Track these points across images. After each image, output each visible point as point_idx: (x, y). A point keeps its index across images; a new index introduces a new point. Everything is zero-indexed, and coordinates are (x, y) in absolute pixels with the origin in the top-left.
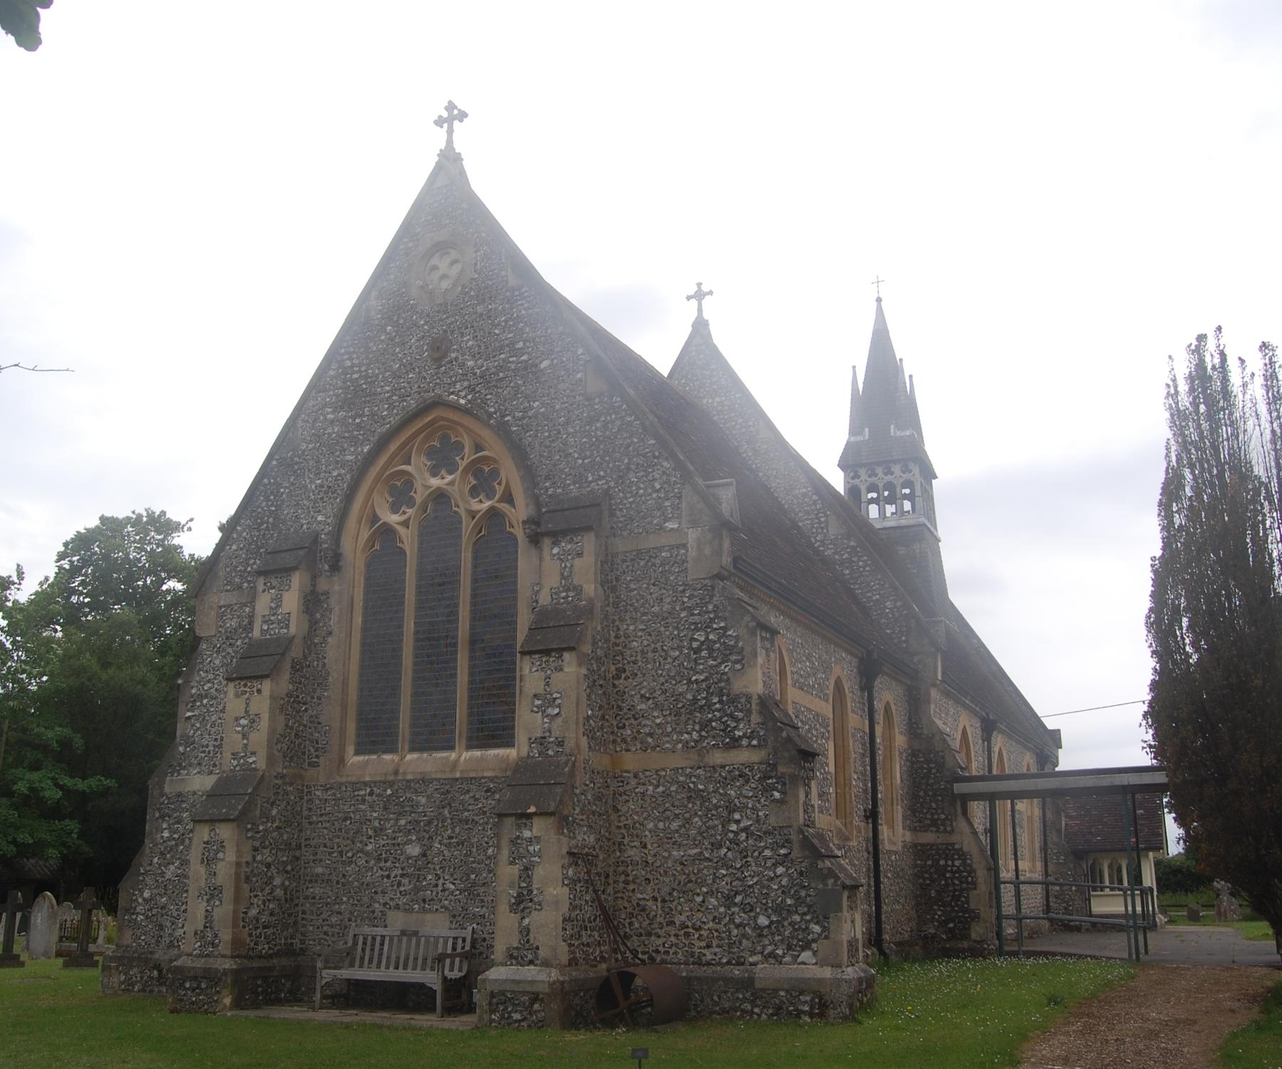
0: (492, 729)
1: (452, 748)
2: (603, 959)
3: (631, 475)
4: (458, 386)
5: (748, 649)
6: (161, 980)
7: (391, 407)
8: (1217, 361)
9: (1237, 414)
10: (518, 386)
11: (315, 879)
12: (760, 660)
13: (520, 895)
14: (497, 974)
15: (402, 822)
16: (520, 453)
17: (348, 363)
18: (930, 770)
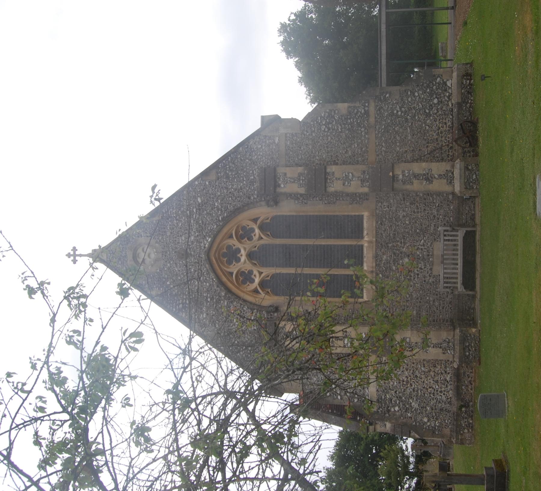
1: (362, 246)
3: (254, 158)
14: (457, 189)
15: (394, 268)
17: (181, 306)
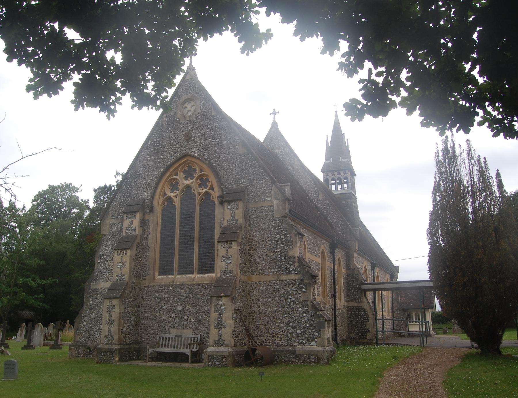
0: (207, 267)
1: (193, 273)
2: (245, 345)
3: (255, 181)
4: (194, 149)
5: (294, 241)
6: (90, 353)
7: (171, 156)
8: (452, 145)
9: (458, 163)
10: (215, 150)
11: (145, 318)
12: (298, 245)
13: (218, 323)
14: (211, 349)
15: (176, 299)
16: (216, 173)
17: (155, 140)
18: (353, 281)
